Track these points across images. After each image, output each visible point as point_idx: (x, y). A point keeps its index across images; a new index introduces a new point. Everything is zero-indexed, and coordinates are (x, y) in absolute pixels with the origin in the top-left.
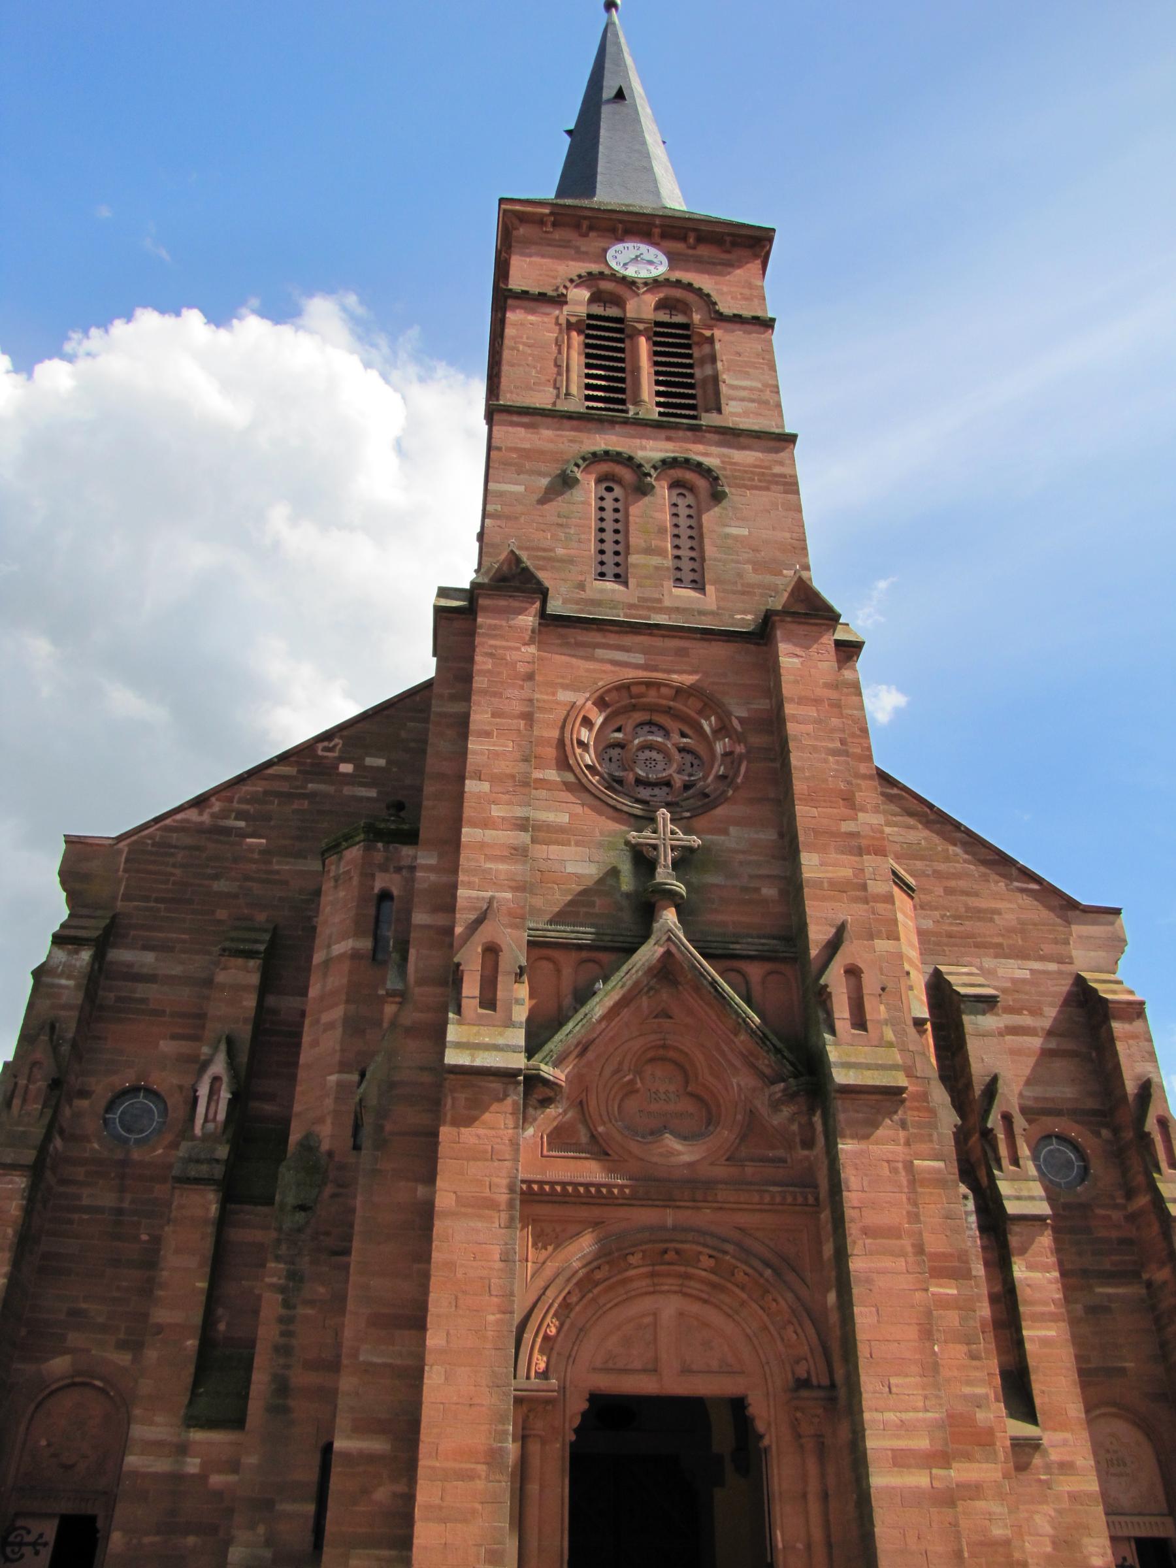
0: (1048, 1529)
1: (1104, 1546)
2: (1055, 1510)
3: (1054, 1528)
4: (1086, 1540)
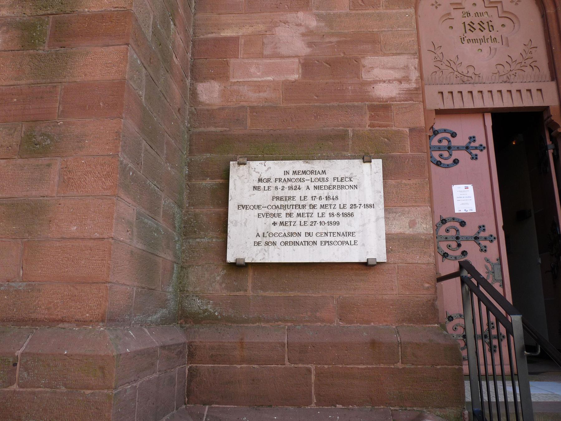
0: (300, 47)
1: (406, 67)
2: (319, 17)
3: (310, 44)
4: (368, 61)
